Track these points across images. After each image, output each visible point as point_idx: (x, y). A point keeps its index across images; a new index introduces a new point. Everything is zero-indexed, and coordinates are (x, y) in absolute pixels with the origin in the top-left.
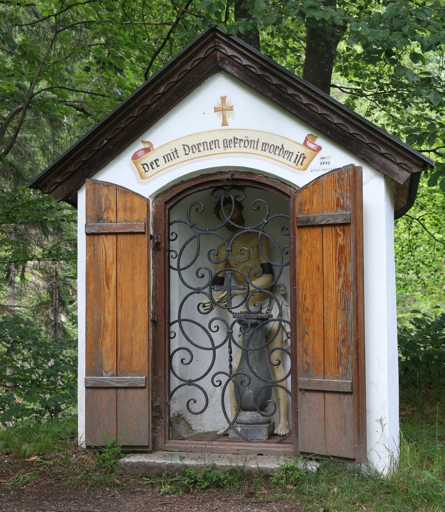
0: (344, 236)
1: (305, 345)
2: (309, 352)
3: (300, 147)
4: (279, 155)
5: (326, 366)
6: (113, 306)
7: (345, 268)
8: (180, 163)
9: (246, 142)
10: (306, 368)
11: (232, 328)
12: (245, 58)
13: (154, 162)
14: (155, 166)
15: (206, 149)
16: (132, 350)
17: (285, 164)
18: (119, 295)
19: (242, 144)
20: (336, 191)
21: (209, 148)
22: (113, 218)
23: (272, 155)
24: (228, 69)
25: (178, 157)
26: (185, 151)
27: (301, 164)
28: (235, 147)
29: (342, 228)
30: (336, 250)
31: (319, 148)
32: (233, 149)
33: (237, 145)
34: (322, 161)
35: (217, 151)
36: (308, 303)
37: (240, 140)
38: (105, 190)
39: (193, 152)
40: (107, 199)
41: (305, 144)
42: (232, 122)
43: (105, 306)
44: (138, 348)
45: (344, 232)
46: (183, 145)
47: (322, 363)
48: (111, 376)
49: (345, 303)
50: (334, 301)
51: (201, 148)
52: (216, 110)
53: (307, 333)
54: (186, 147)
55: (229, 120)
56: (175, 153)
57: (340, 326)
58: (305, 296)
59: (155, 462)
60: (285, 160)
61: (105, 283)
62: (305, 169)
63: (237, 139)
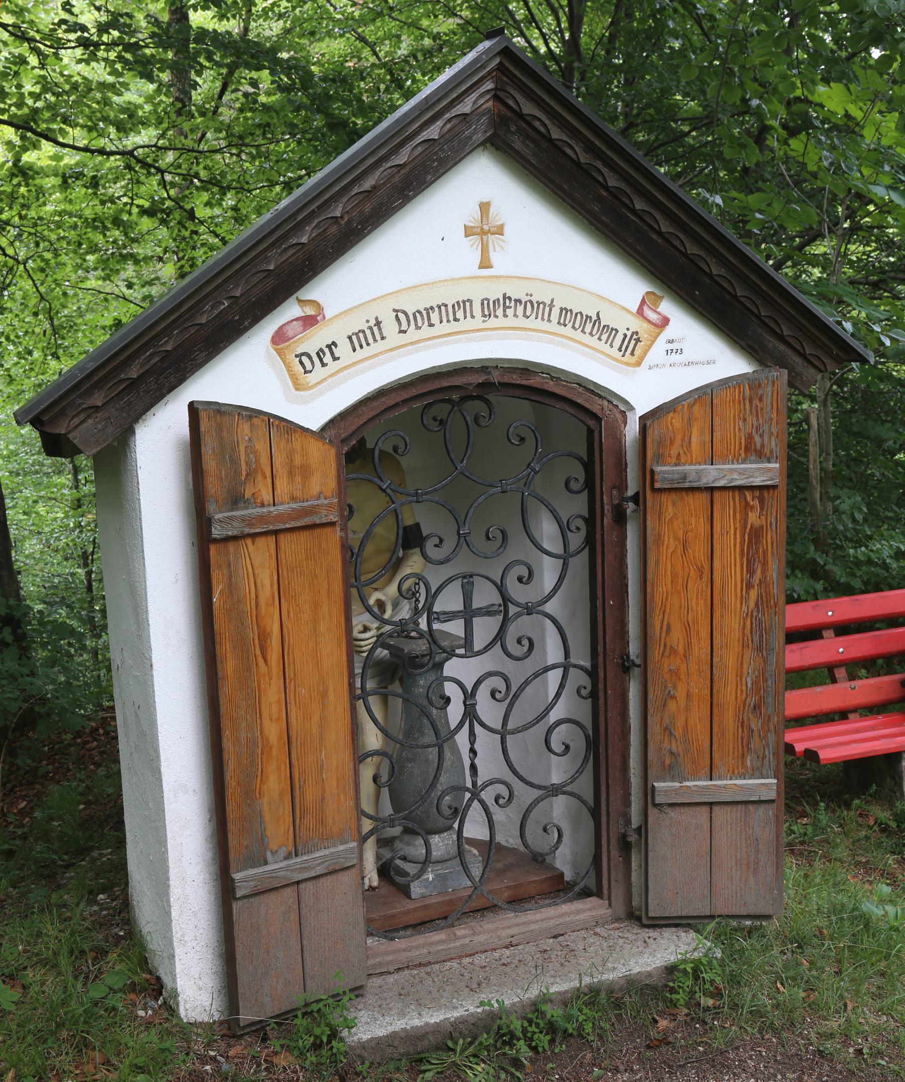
0: (762, 509)
1: (666, 721)
2: (676, 734)
3: (629, 317)
4: (591, 334)
5: (716, 756)
6: (279, 701)
7: (764, 571)
8: (387, 351)
9: (529, 305)
10: (668, 762)
11: (473, 694)
12: (554, 124)
13: (327, 350)
14: (328, 358)
15: (444, 320)
16: (324, 790)
17: (602, 352)
18: (290, 673)
19: (520, 309)
20: (745, 420)
21: (451, 318)
22: (267, 497)
23: (578, 335)
24: (518, 144)
25: (383, 338)
26: (400, 324)
27: (632, 354)
28: (505, 316)
29: (757, 493)
30: (743, 536)
31: (666, 321)
32: (501, 322)
33: (510, 312)
34: (670, 346)
35: (466, 324)
36: (677, 638)
37: (516, 301)
38: (245, 429)
39: (418, 328)
40: (250, 450)
41: (640, 312)
42: (501, 262)
43: (263, 704)
44: (335, 783)
45: (762, 501)
46: (395, 310)
47: (708, 751)
48: (286, 858)
49: (761, 636)
50: (737, 634)
51: (435, 317)
52: (469, 232)
53: (673, 697)
54: (401, 315)
55: (495, 257)
56: (375, 329)
57: (749, 680)
58: (669, 625)
59: (427, 1024)
60: (602, 346)
61: (258, 652)
62: (638, 364)
63: (510, 298)
